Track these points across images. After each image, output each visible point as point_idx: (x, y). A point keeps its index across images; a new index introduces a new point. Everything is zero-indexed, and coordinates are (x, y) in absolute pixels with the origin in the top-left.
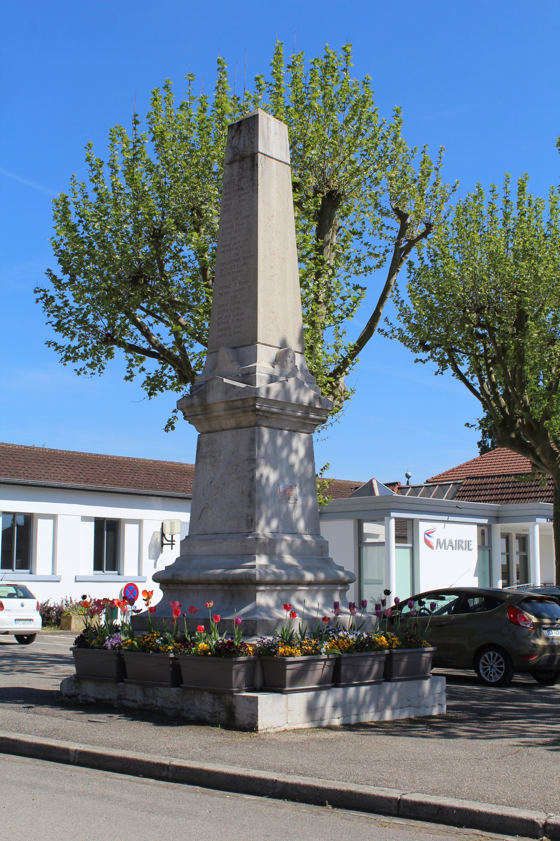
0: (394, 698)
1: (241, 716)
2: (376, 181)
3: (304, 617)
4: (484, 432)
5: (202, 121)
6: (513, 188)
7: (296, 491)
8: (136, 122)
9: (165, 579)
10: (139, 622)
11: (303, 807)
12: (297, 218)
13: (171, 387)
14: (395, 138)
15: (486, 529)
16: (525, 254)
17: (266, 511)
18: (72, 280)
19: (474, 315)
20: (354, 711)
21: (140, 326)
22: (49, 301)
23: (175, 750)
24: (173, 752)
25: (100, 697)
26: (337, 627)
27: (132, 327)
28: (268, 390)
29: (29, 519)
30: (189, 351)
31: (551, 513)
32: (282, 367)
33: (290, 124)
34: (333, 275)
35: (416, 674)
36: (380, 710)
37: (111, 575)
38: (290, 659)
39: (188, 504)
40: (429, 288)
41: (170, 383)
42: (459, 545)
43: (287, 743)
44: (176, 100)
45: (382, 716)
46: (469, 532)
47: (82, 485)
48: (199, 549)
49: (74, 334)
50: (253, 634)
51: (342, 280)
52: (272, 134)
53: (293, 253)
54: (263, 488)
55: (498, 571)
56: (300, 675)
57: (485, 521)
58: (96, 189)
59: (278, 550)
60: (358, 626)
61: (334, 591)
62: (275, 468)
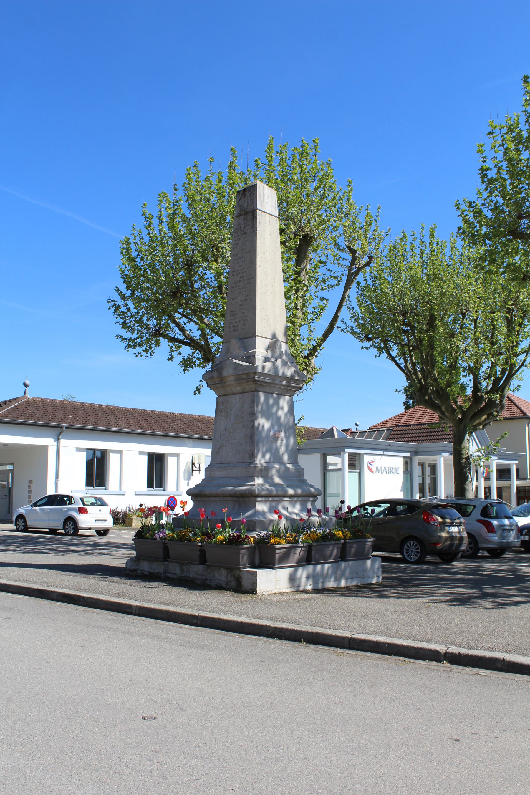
25: (152, 571)
57: (408, 455)
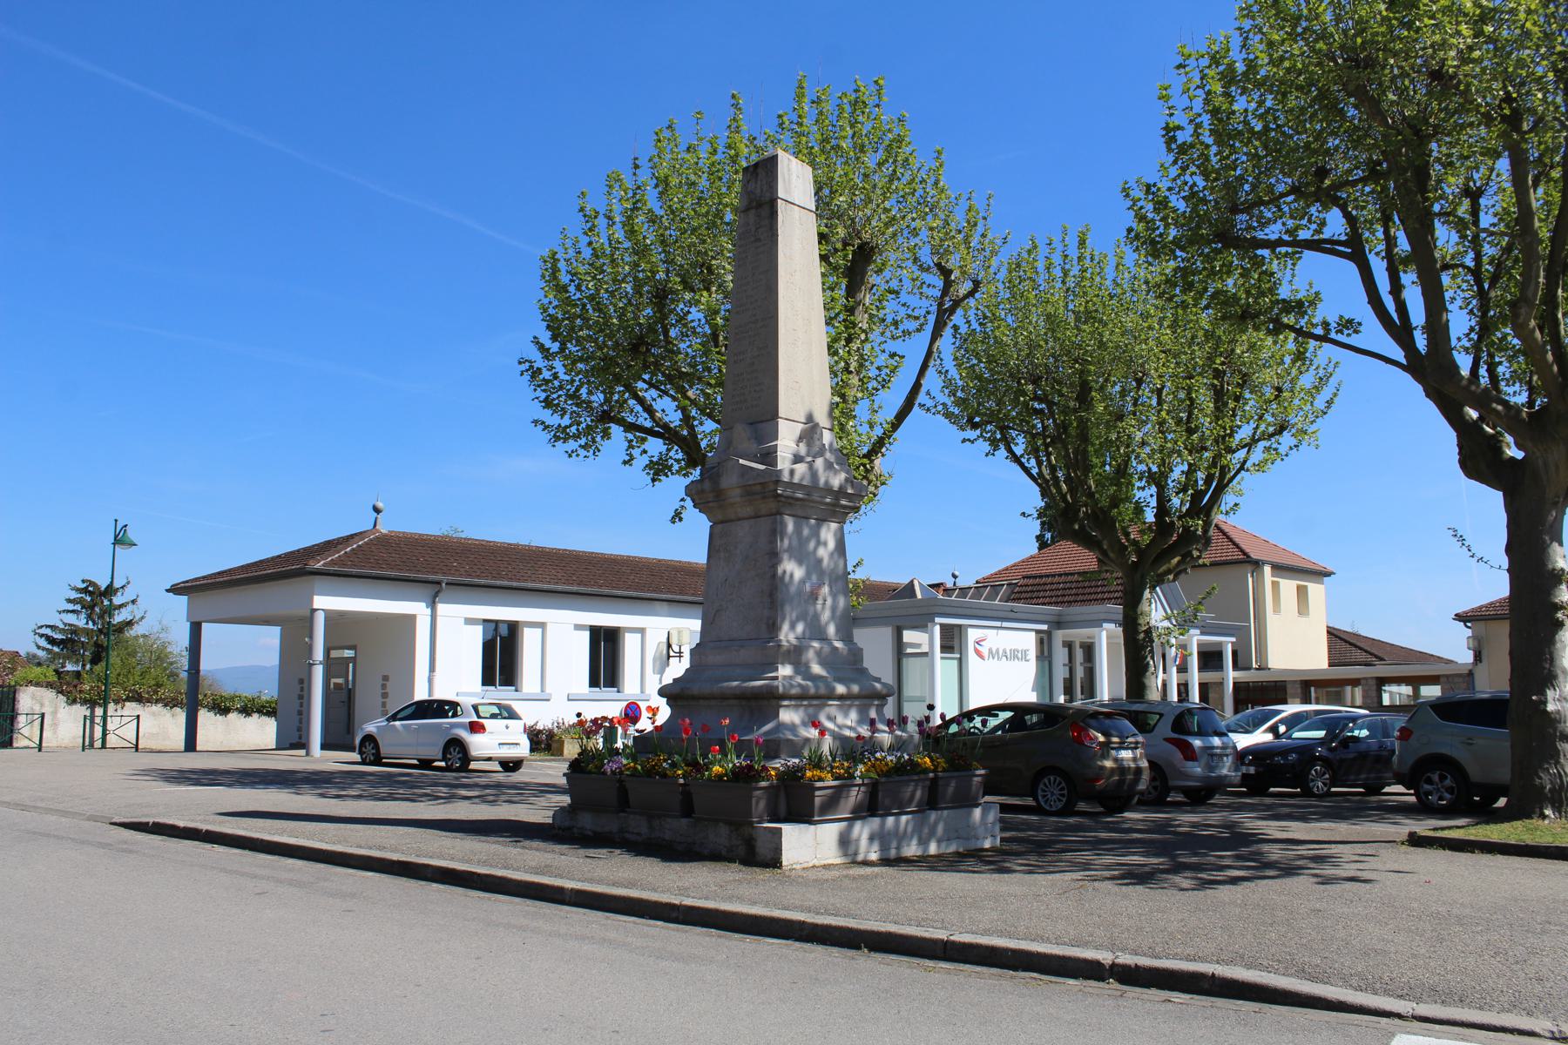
0: (940, 829)
1: (762, 849)
2: (915, 232)
3: (837, 737)
4: (1043, 524)
5: (713, 164)
6: (1072, 242)
7: (826, 589)
8: (636, 167)
9: (671, 693)
10: (642, 740)
11: (835, 951)
12: (823, 275)
13: (678, 472)
14: (936, 183)
15: (1045, 636)
16: (1088, 316)
17: (790, 613)
18: (562, 349)
19: (1030, 387)
20: (894, 844)
21: (641, 401)
22: (536, 373)
23: (687, 889)
24: (683, 891)
26: (871, 746)
27: (632, 402)
28: (792, 472)
29: (514, 628)
30: (699, 429)
31: (1120, 617)
32: (809, 445)
33: (813, 164)
34: (867, 339)
35: (966, 801)
36: (923, 842)
37: (610, 692)
38: (819, 784)
39: (699, 610)
40: (977, 356)
41: (676, 467)
42: (1015, 655)
43: (816, 880)
44: (683, 142)
45: (926, 849)
46: (1025, 640)
47: (575, 588)
48: (714, 658)
49: (564, 412)
50: (776, 756)
51: (877, 347)
52: (794, 177)
53: (819, 315)
54: (787, 586)
55: (1059, 686)
56: (831, 804)
57: (1045, 627)
58: (590, 243)
59: (804, 659)
60: (899, 745)
61: (870, 705)
62: (800, 562)
